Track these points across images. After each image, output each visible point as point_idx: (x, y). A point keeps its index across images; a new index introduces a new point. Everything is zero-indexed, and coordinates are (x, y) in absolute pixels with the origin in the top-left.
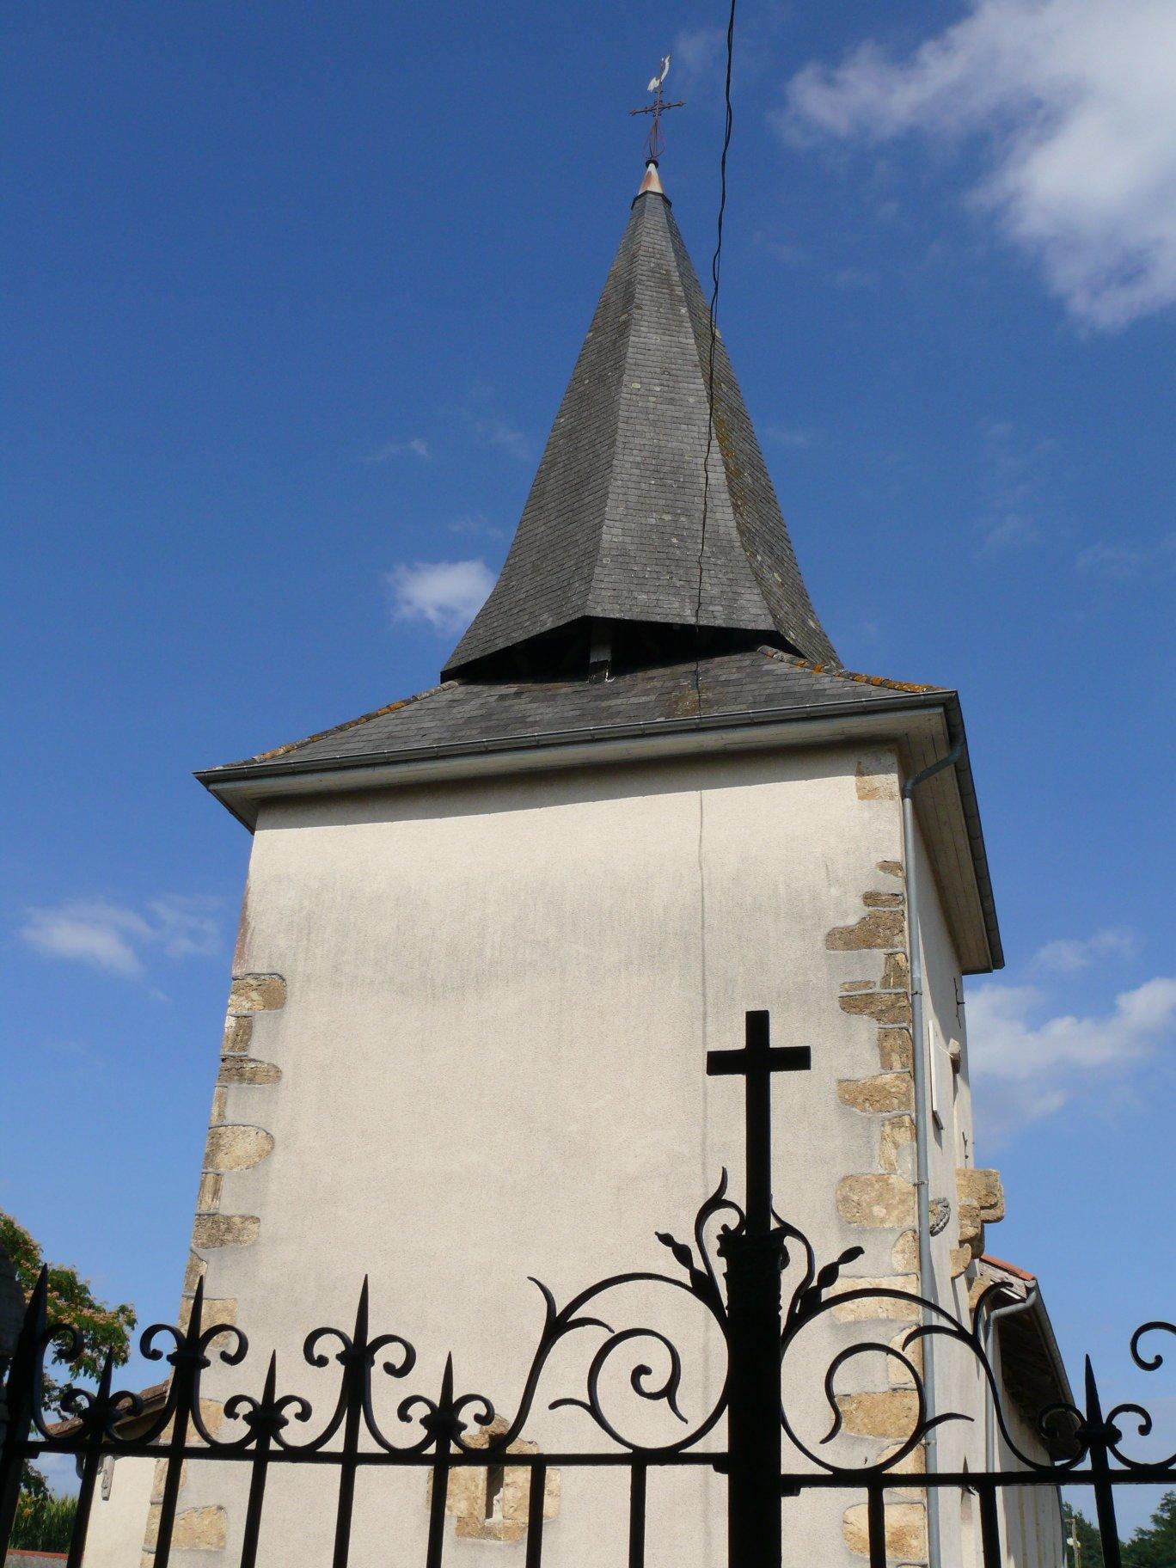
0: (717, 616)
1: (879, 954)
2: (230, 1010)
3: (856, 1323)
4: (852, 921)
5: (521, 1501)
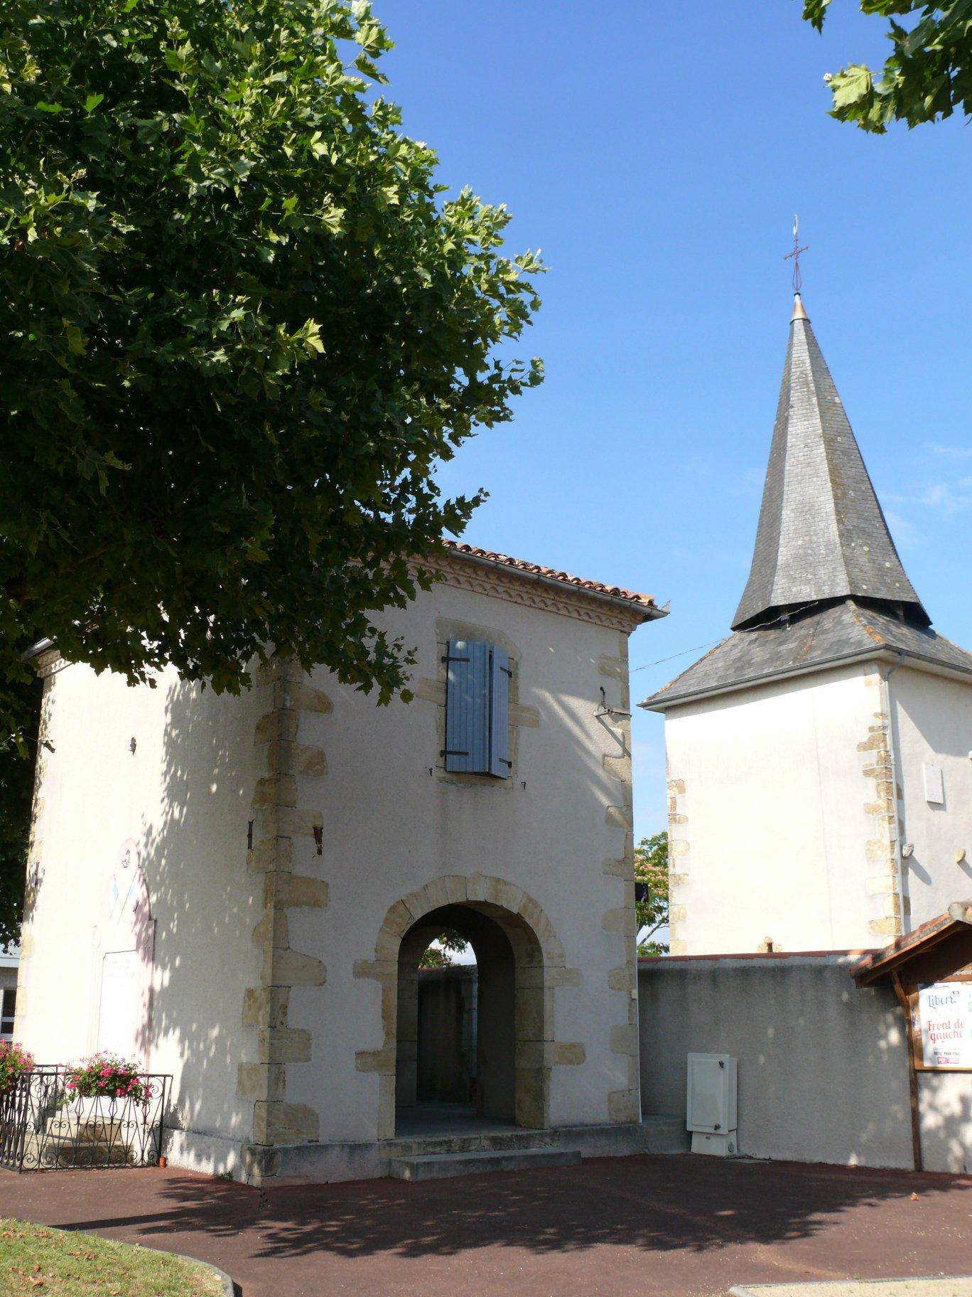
0: (826, 593)
1: (875, 751)
2: (668, 796)
3: (874, 895)
4: (865, 739)
5: (645, 847)
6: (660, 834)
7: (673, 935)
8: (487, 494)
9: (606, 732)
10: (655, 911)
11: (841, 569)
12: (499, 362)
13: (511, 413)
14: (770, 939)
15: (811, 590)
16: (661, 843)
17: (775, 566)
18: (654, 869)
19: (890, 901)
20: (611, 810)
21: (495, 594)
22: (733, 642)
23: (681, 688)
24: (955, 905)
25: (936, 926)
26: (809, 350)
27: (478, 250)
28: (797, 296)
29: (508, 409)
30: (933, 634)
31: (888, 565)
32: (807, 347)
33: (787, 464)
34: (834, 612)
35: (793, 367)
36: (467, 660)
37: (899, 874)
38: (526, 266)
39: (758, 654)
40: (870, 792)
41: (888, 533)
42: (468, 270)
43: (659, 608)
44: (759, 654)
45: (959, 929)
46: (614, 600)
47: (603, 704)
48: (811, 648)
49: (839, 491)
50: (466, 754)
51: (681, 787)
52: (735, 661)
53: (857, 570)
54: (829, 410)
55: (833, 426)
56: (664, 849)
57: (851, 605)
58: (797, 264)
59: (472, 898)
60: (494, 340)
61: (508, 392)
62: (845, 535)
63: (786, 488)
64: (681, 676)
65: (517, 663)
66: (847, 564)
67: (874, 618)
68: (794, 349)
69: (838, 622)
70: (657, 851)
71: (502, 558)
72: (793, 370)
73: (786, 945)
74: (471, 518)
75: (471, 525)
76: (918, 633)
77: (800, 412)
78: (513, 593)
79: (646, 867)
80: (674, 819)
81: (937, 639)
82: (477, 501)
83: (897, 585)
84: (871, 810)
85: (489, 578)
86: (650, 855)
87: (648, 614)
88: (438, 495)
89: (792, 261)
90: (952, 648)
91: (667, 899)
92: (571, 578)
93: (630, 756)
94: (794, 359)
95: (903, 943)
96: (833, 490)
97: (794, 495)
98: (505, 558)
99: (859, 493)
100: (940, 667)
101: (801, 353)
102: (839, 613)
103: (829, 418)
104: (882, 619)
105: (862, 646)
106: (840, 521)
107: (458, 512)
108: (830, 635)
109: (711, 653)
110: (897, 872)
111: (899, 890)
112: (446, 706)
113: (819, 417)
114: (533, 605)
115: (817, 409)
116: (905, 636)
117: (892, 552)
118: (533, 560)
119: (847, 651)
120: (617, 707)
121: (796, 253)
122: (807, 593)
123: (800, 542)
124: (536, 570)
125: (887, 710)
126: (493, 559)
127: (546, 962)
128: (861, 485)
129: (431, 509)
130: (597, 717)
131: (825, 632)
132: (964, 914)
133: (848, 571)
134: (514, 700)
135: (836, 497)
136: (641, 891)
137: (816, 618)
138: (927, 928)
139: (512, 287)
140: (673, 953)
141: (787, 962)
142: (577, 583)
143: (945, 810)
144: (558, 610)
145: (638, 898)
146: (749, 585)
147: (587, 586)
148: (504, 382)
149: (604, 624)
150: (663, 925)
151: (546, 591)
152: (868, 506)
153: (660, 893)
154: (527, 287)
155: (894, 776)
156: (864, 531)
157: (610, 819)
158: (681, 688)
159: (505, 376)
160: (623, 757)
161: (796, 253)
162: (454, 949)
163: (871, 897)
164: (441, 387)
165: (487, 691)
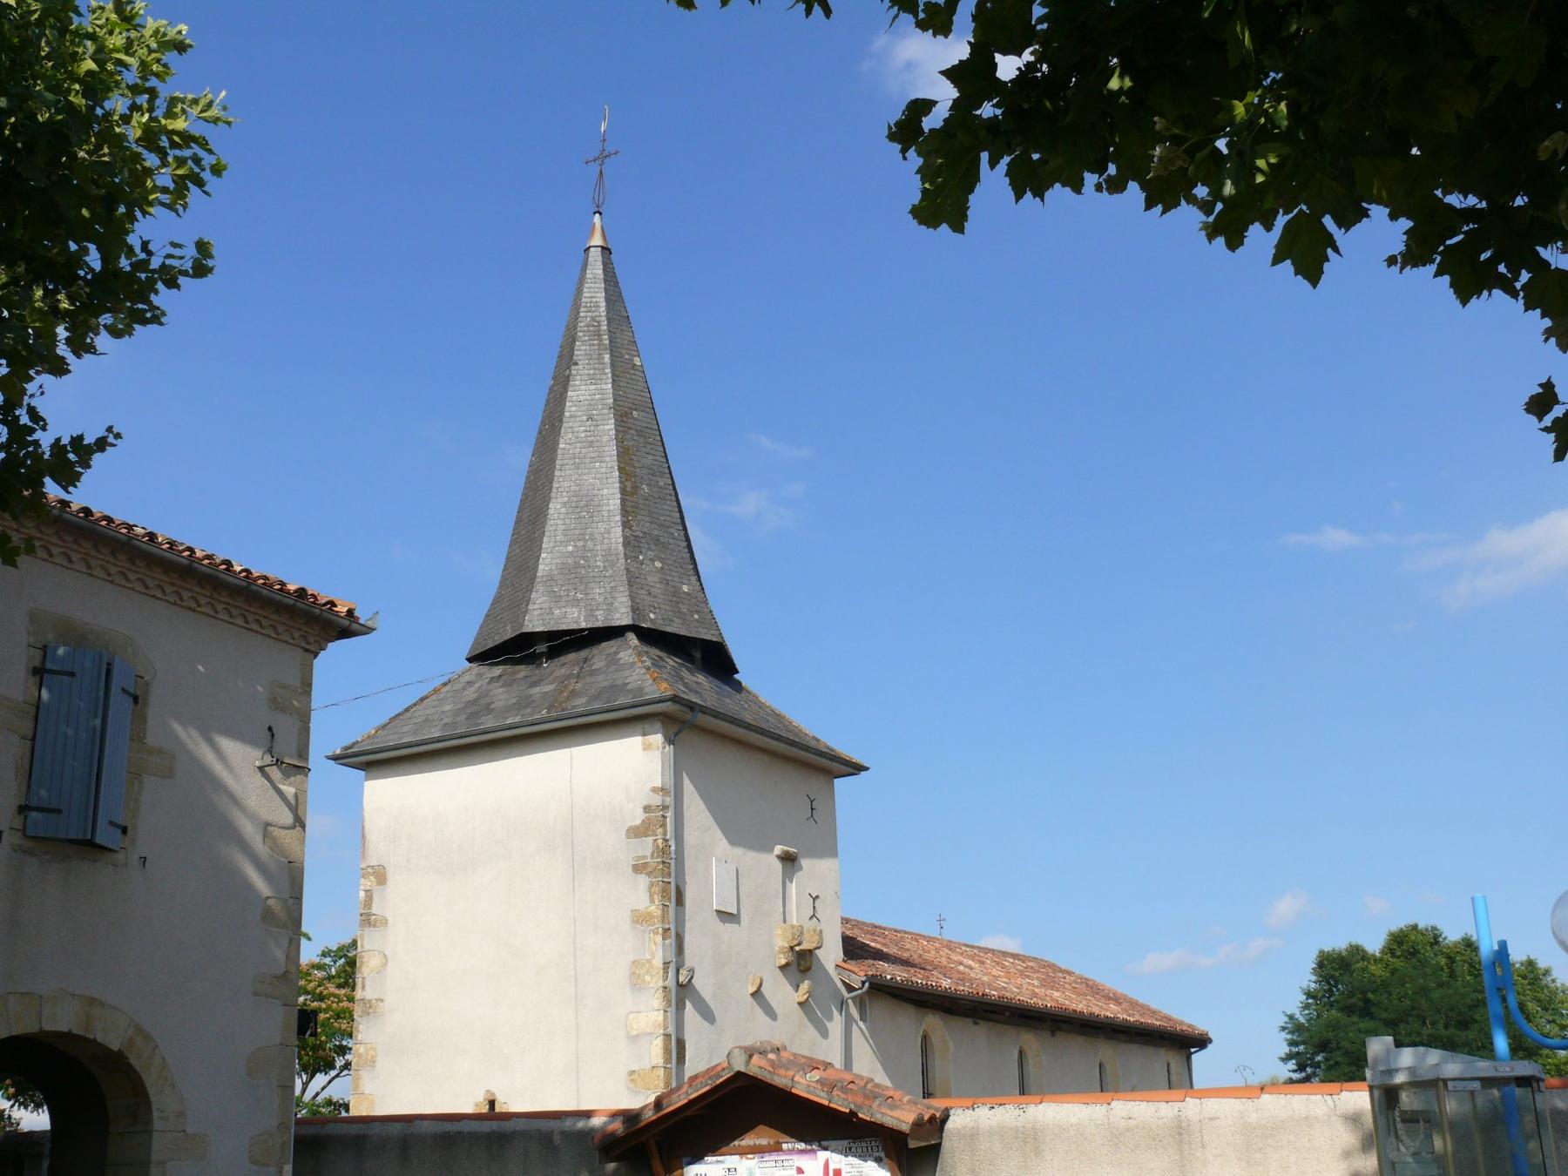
1: (650, 840)
2: (362, 887)
3: (638, 1035)
4: (638, 822)
5: (328, 960)
6: (350, 941)
7: (356, 1087)
8: (118, 436)
9: (271, 791)
10: (335, 1052)
11: (622, 589)
12: (148, 242)
13: (164, 314)
14: (493, 1094)
15: (580, 614)
16: (350, 955)
17: (535, 576)
18: (337, 992)
19: (659, 1043)
20: (271, 902)
21: (123, 582)
22: (467, 678)
23: (391, 737)
24: (737, 1051)
25: (710, 1078)
26: (606, 290)
27: (131, 77)
28: (597, 215)
29: (158, 308)
30: (738, 687)
31: (685, 588)
32: (603, 285)
33: (561, 441)
34: (609, 647)
35: (582, 309)
36: (72, 674)
37: (672, 1009)
38: (202, 111)
39: (501, 696)
40: (640, 895)
41: (689, 547)
42: (118, 104)
43: (361, 621)
44: (502, 697)
45: (738, 1084)
46: (299, 604)
47: (270, 751)
48: (574, 694)
49: (628, 484)
50: (59, 811)
51: (380, 876)
52: (469, 704)
53: (644, 592)
54: (625, 373)
55: (629, 396)
56: (352, 963)
57: (632, 638)
58: (601, 171)
59: (48, 1026)
60: (145, 213)
61: (160, 286)
62: (632, 544)
63: (557, 473)
64: (392, 719)
65: (147, 684)
66: (630, 583)
67: (660, 657)
68: (587, 285)
69: (613, 661)
70: (344, 966)
71: (139, 530)
72: (581, 314)
73: (517, 1101)
74: (89, 467)
75: (88, 478)
76: (718, 682)
77: (586, 372)
78: (151, 583)
79: (327, 988)
80: (368, 920)
81: (743, 694)
82: (101, 444)
83: (696, 616)
84: (639, 919)
85: (116, 558)
86: (333, 971)
87: (345, 627)
88: (44, 429)
89: (594, 168)
90: (761, 706)
91: (351, 1036)
92: (238, 569)
93: (303, 826)
94: (583, 300)
95: (665, 1102)
96: (621, 482)
97: (566, 484)
98: (143, 531)
99: (655, 489)
100: (743, 731)
101: (594, 292)
102: (615, 648)
103: (624, 384)
104: (671, 661)
105: (641, 696)
106: (626, 525)
107: (71, 456)
108: (601, 678)
109: (436, 691)
110: (670, 1006)
111: (671, 1030)
112: (33, 739)
113: (610, 380)
114: (179, 602)
115: (608, 371)
116: (702, 687)
117: (692, 572)
118: (185, 538)
119: (622, 701)
120: (291, 757)
121: (603, 157)
122: (574, 618)
123: (570, 548)
124: (187, 553)
125: (670, 784)
126: (124, 531)
127: (157, 1124)
128: (658, 479)
129: (31, 449)
130: (261, 769)
131: (593, 673)
132: (748, 1062)
133: (631, 592)
134: (138, 736)
135: (623, 491)
136: (306, 1020)
137: (584, 653)
138: (698, 1081)
139: (176, 139)
140: (354, 1112)
141: (509, 1126)
142: (246, 577)
143: (739, 923)
144: (216, 612)
145: (302, 1030)
146: (496, 601)
147: (261, 581)
148: (154, 271)
149: (281, 637)
150: (345, 1072)
151: (200, 583)
152: (666, 507)
153: (344, 1027)
154: (203, 143)
155: (673, 874)
156: (657, 541)
157: (268, 916)
158: (391, 737)
159: (155, 263)
160: (294, 827)
161: (603, 157)
162: (26, 1108)
163: (634, 1039)
164: (64, 272)
165: (98, 722)
